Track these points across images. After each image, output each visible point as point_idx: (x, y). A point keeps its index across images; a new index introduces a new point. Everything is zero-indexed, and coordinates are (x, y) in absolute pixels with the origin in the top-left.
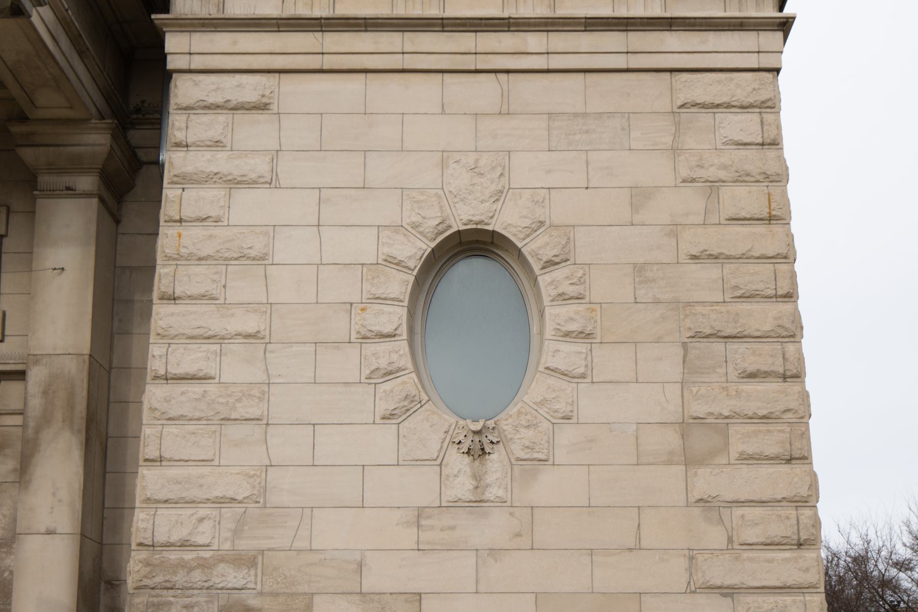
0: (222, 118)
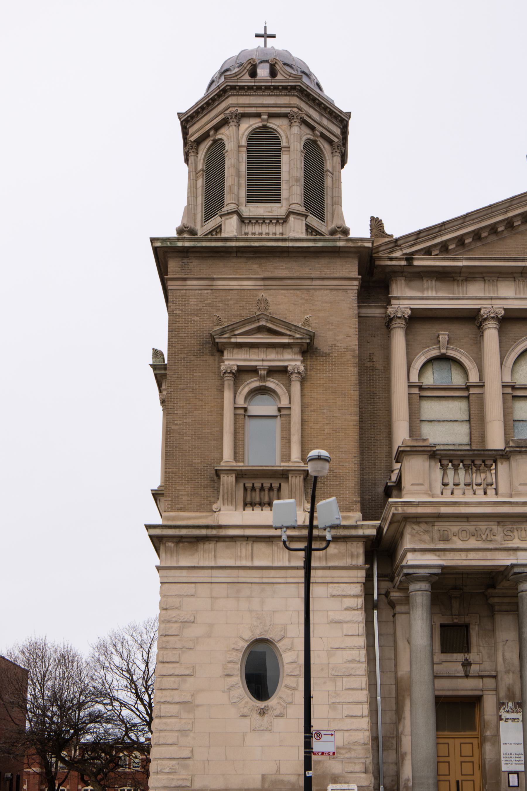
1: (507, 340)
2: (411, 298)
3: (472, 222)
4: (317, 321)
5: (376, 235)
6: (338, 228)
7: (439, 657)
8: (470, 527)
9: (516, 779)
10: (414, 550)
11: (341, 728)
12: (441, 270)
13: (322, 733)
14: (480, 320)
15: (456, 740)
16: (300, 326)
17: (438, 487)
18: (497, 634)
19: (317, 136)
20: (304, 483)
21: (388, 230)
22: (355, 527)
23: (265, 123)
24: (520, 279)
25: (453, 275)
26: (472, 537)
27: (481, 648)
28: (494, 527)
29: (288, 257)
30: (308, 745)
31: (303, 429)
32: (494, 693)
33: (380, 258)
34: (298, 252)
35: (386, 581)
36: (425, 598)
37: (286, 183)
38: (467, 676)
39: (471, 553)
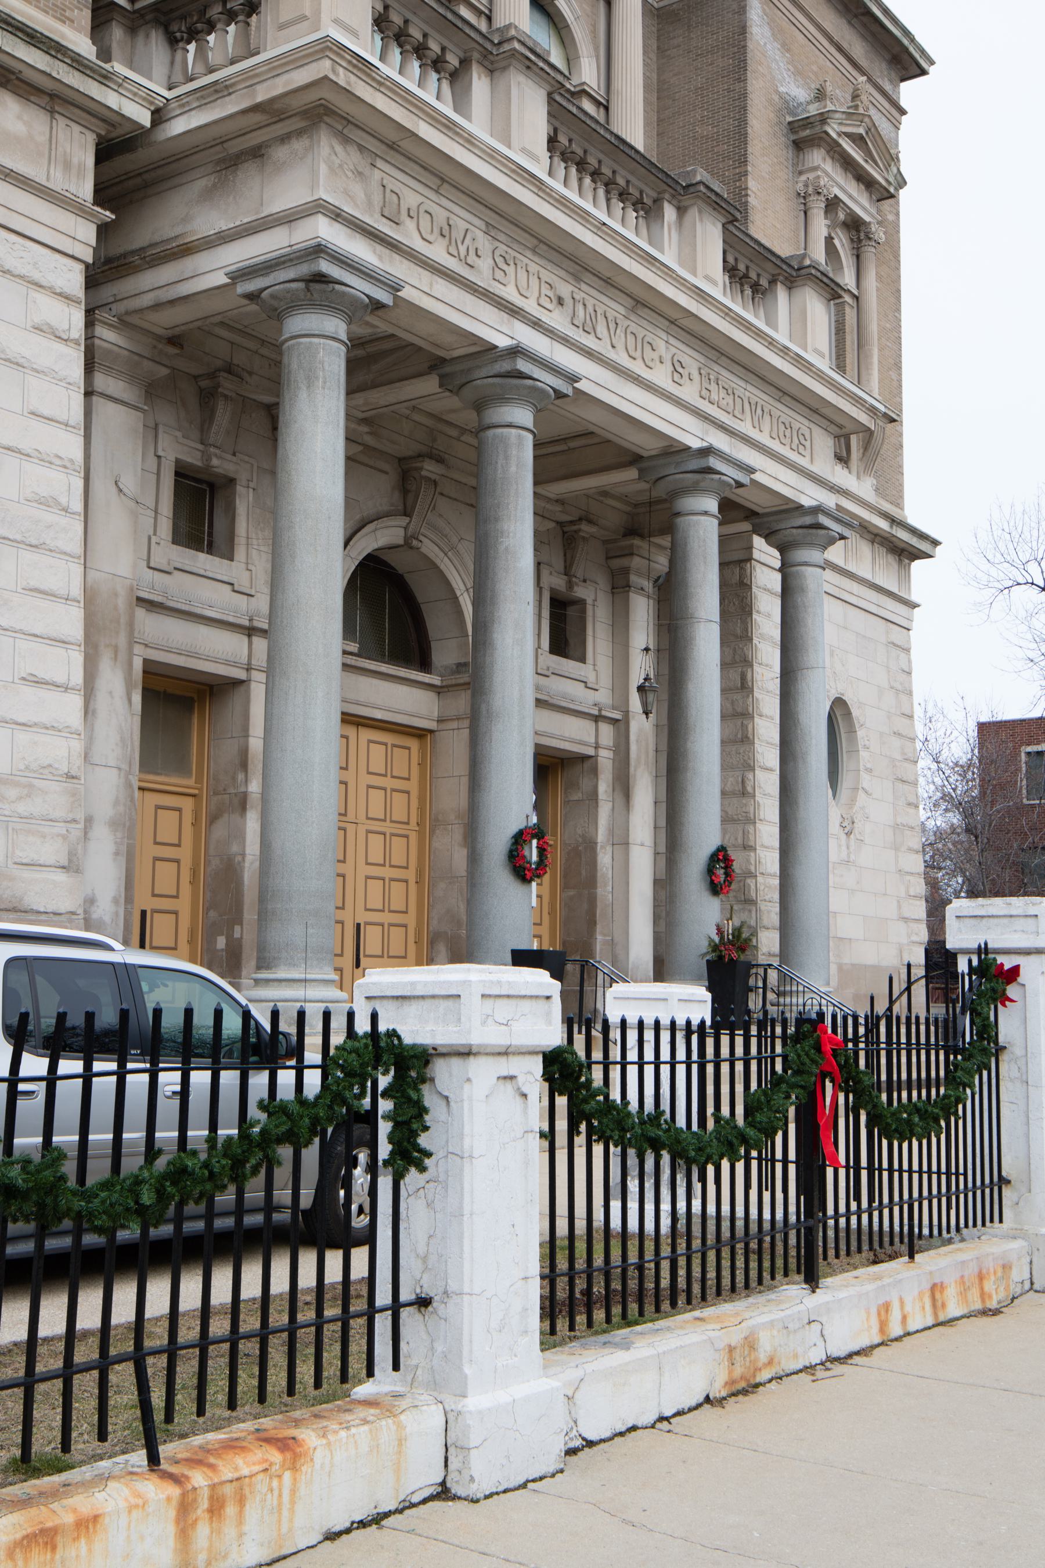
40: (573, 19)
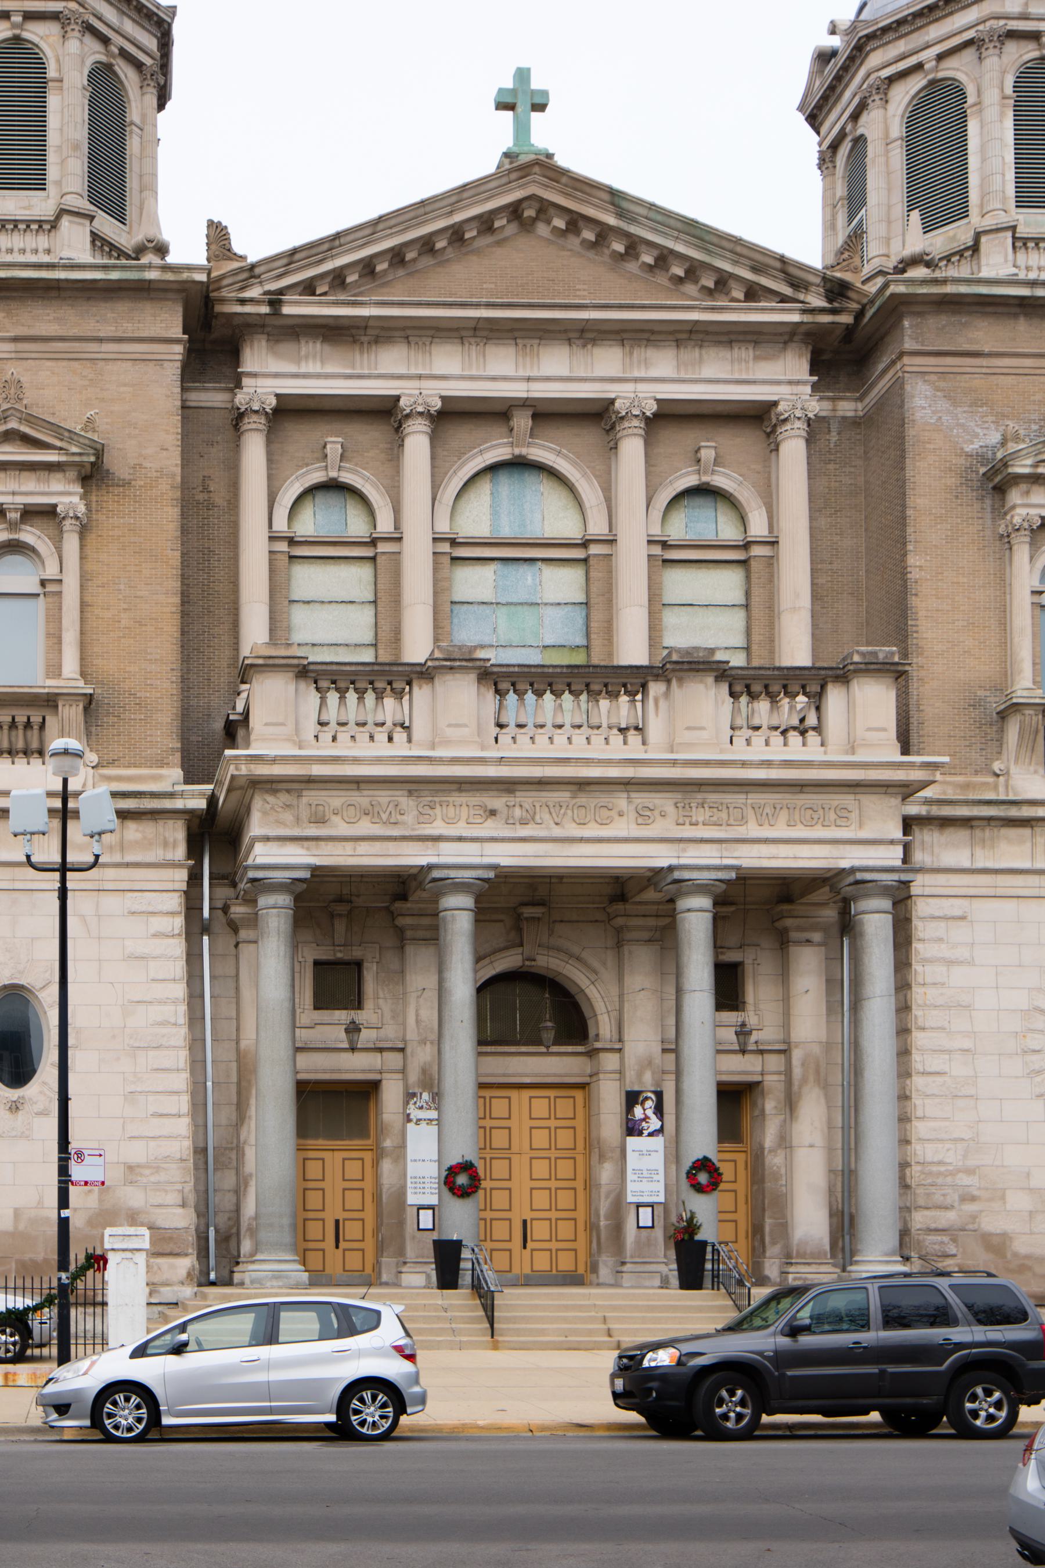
0: (943, 924)
1: (445, 453)
2: (276, 375)
3: (389, 231)
4: (109, 420)
5: (217, 256)
6: (149, 241)
7: (308, 1015)
8: (362, 798)
9: (431, 1219)
10: (267, 839)
11: (143, 1134)
12: (331, 322)
13: (86, 1152)
14: (400, 417)
15: (336, 1153)
16: (77, 431)
17: (310, 727)
18: (408, 978)
19: (114, 57)
20: (85, 716)
21: (238, 246)
22: (171, 795)
23: (17, 32)
24: (472, 340)
25: (354, 331)
26: (365, 817)
27: (381, 1001)
28: (400, 799)
29: (59, 297)
30: (63, 1170)
31: (83, 620)
32: (400, 1076)
33: (223, 301)
34: (77, 289)
35: (224, 885)
36: (282, 921)
37: (55, 152)
38: (353, 1049)
39: (362, 843)
40: (735, 486)
